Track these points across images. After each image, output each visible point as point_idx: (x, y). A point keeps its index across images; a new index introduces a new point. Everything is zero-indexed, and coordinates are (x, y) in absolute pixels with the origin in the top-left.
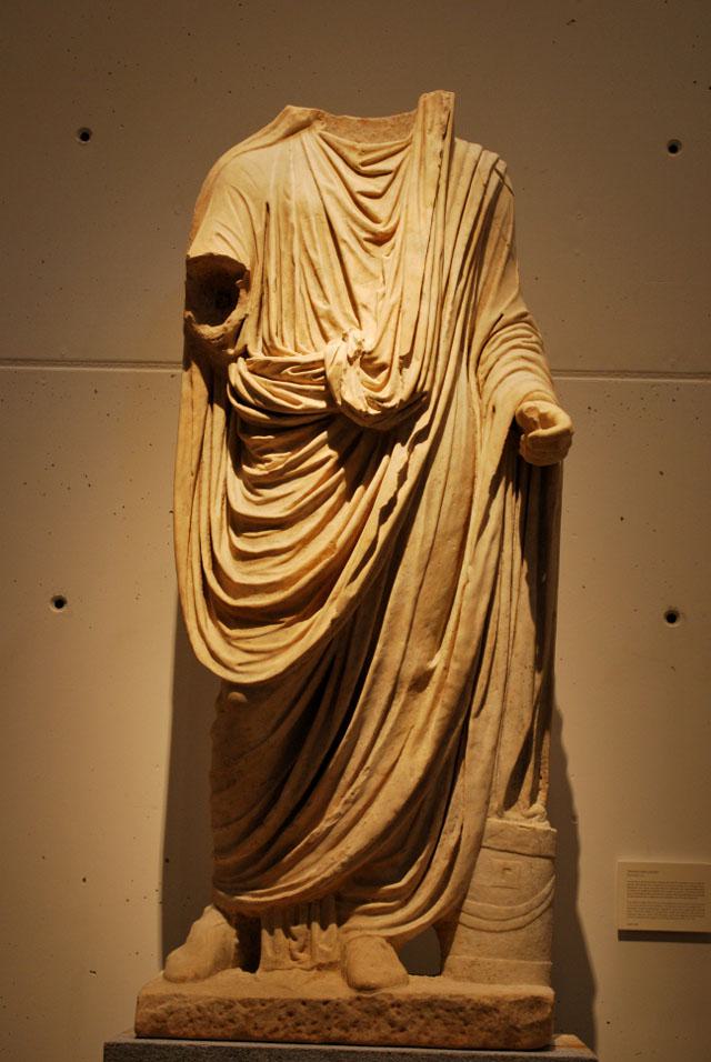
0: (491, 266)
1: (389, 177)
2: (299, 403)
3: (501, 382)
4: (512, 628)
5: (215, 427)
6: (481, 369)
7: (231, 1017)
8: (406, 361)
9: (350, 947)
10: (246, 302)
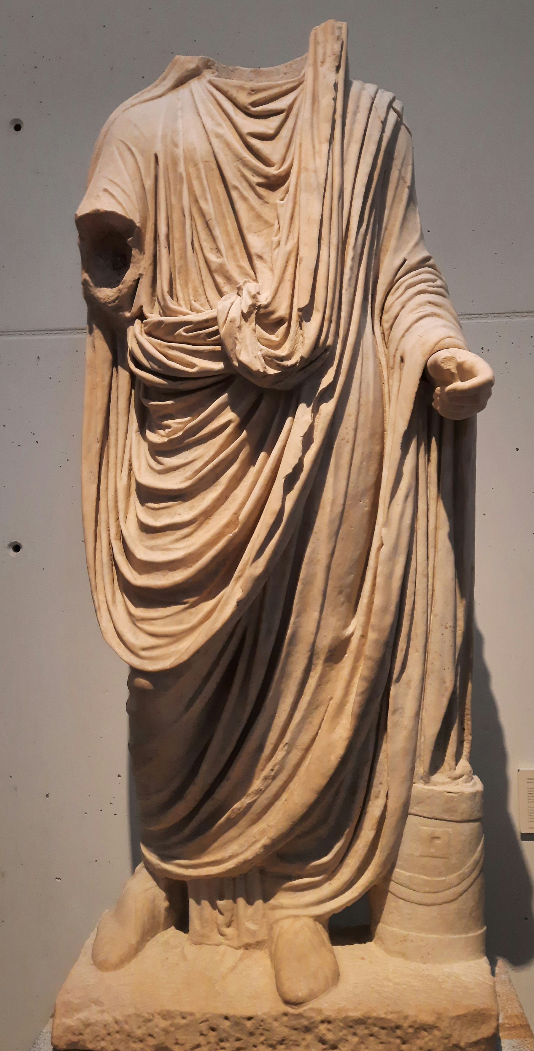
1: (282, 116)
2: (193, 366)
3: (407, 330)
4: (430, 587)
5: (120, 391)
6: (385, 317)
8: (306, 313)
9: (277, 929)
10: (138, 262)
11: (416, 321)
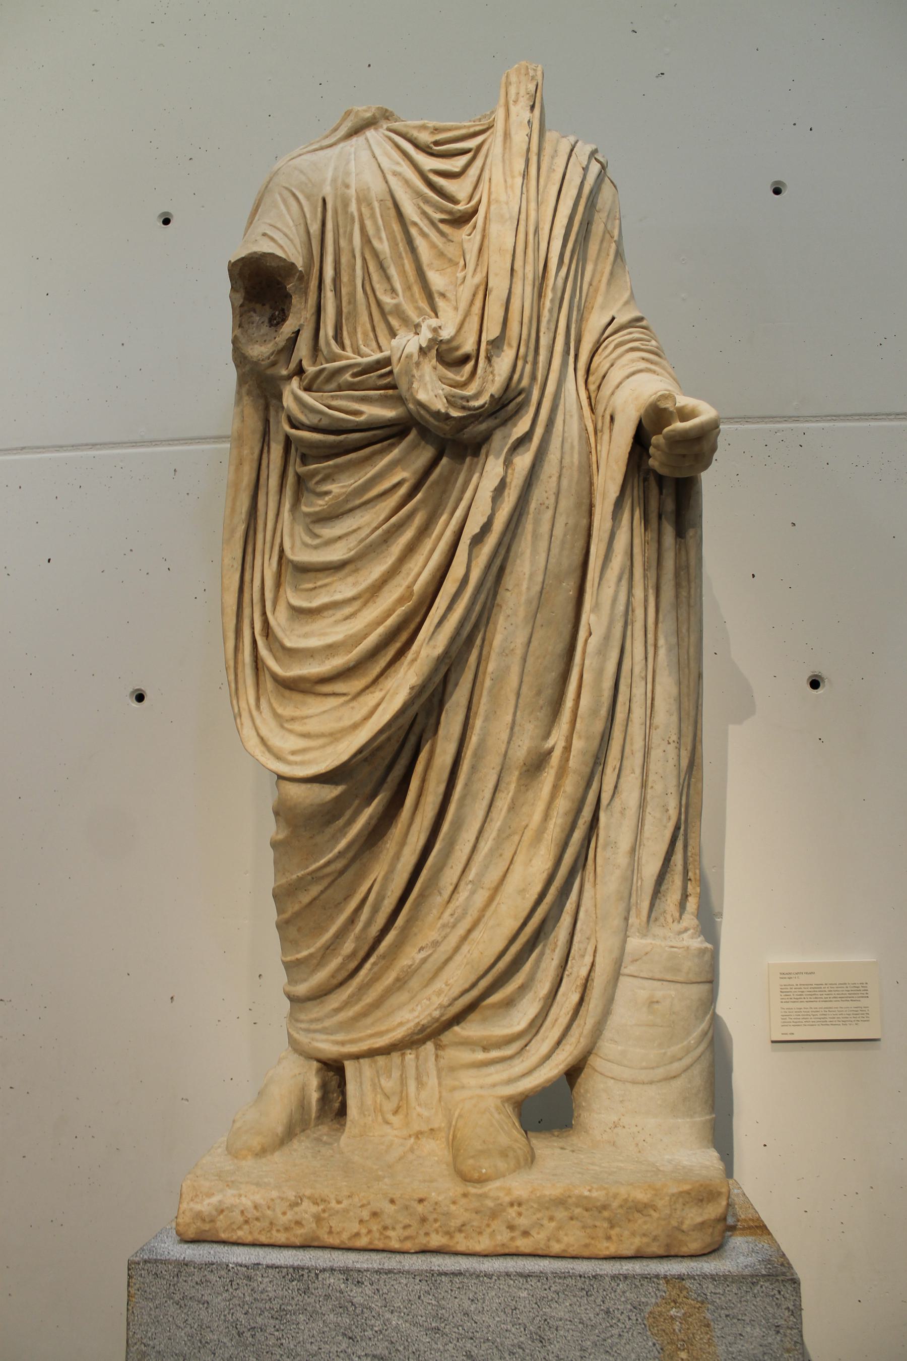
0: (596, 265)
1: (469, 155)
3: (618, 387)
6: (591, 379)
7: (298, 1218)
8: (497, 344)
11: (628, 377)
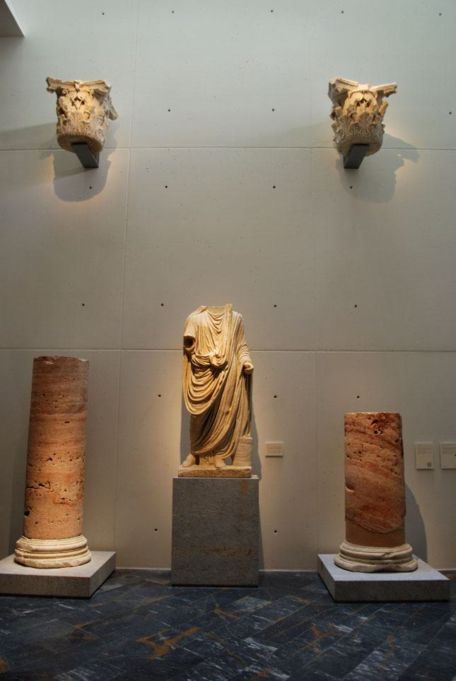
8: (224, 356)
